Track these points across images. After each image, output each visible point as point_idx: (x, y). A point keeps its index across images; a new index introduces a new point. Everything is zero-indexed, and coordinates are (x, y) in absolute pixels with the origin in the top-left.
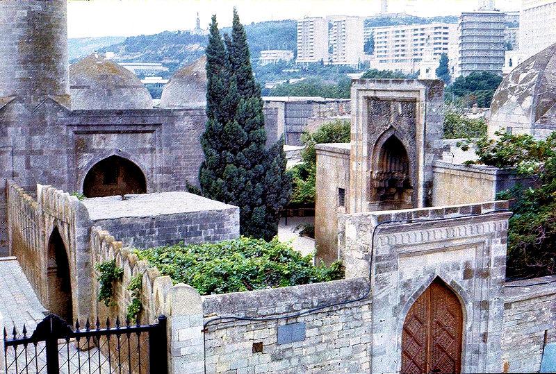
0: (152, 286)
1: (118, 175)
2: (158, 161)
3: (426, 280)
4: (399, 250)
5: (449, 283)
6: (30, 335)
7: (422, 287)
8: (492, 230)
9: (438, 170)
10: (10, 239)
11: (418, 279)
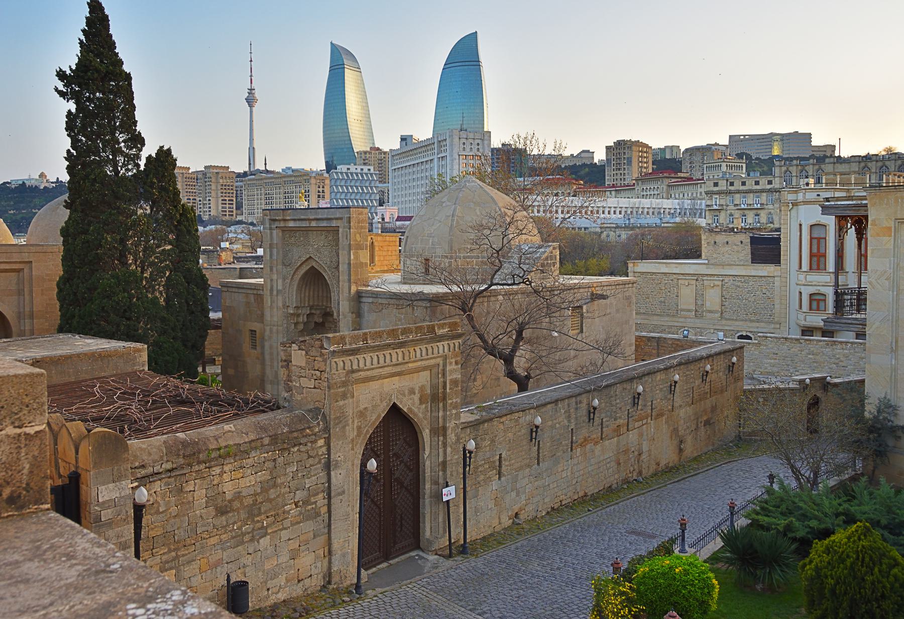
0: (77, 453)
1: (693, 222)
2: (456, 167)
3: (382, 410)
4: (354, 375)
5: (405, 410)
7: (379, 415)
9: (364, 300)
11: (375, 407)
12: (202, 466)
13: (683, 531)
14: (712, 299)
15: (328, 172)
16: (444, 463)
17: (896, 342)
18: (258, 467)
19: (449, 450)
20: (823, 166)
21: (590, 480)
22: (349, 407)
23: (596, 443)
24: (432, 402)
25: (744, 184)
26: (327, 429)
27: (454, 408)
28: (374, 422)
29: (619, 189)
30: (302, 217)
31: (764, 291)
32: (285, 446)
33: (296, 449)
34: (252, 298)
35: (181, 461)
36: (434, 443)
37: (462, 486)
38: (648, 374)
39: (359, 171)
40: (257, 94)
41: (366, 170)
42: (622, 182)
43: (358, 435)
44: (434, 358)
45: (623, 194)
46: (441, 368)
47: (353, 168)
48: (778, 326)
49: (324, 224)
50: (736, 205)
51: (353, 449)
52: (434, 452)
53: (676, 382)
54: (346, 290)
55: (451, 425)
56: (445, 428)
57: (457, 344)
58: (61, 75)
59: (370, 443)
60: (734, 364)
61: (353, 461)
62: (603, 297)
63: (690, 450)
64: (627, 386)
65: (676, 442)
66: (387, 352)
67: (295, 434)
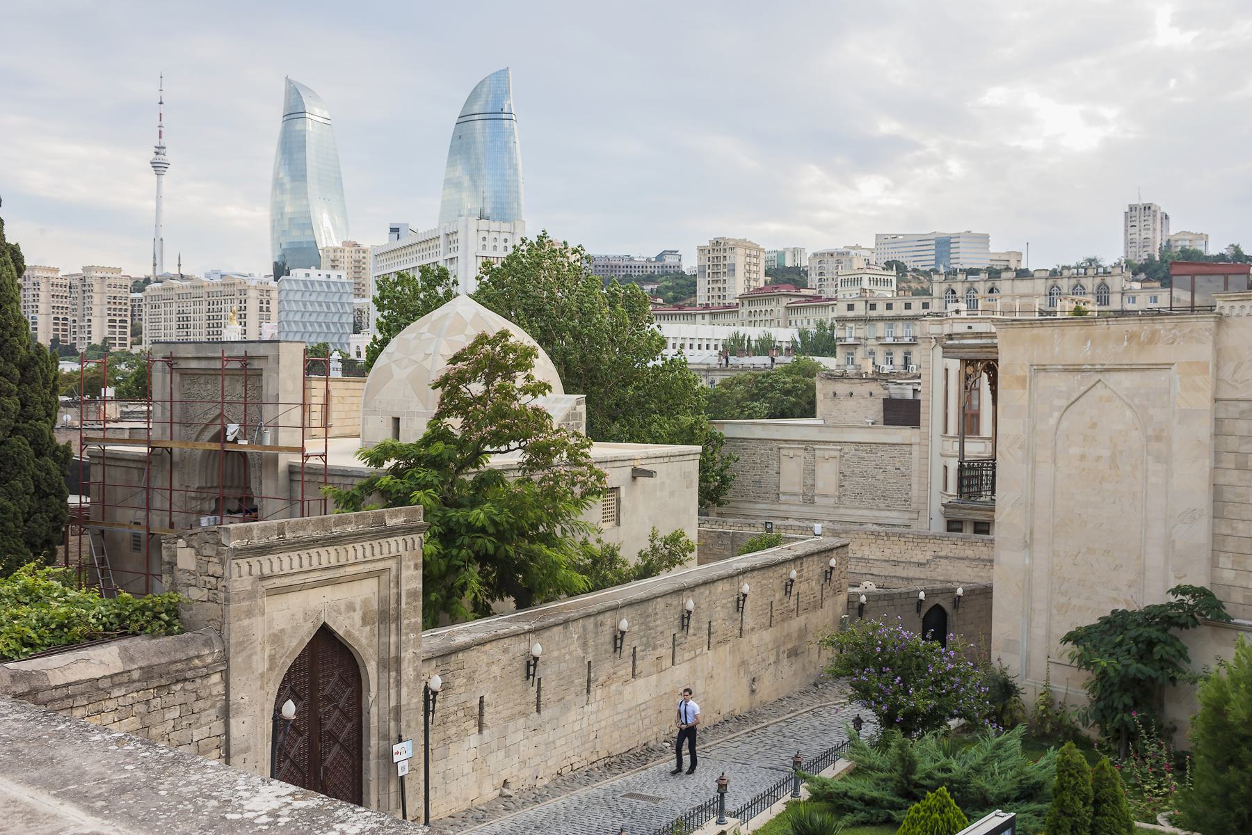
3: (307, 632)
4: (267, 584)
5: (341, 633)
7: (302, 640)
11: (296, 628)
13: (722, 795)
14: (827, 477)
15: (276, 280)
16: (398, 709)
17: (1031, 533)
18: (122, 714)
19: (404, 691)
20: (997, 284)
21: (616, 735)
22: (259, 628)
24: (380, 622)
25: (889, 307)
26: (225, 660)
27: (412, 631)
28: (294, 650)
29: (715, 312)
30: (211, 355)
31: (898, 465)
33: (179, 686)
36: (383, 681)
37: (423, 742)
39: (323, 278)
41: (334, 278)
42: (721, 302)
43: (271, 669)
44: (384, 559)
45: (721, 319)
46: (394, 573)
47: (314, 273)
48: (915, 516)
50: (878, 338)
51: (262, 688)
52: (384, 694)
53: (745, 596)
55: (407, 655)
56: (398, 660)
57: (417, 540)
59: (290, 680)
60: (832, 568)
61: (263, 705)
62: (650, 474)
63: (768, 689)
64: (675, 601)
65: (745, 681)
66: (313, 552)
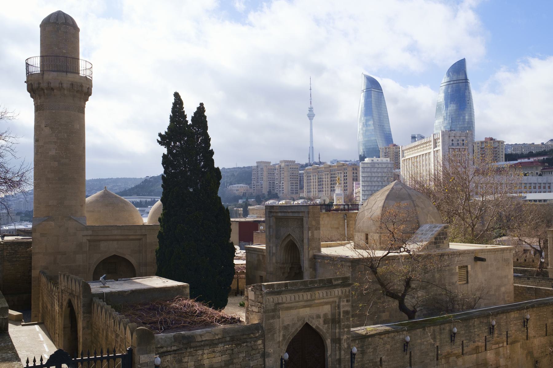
3: (299, 326)
4: (280, 306)
5: (314, 327)
6: (44, 362)
7: (297, 329)
8: (340, 293)
10: (41, 311)
12: (192, 350)
18: (223, 353)
19: (343, 352)
23: (458, 357)
24: (332, 323)
32: (238, 342)
33: (245, 344)
34: (261, 257)
35: (181, 346)
38: (503, 312)
40: (315, 111)
46: (337, 303)
49: (296, 215)
51: (279, 347)
54: (307, 255)
58: (160, 135)
67: (245, 336)
